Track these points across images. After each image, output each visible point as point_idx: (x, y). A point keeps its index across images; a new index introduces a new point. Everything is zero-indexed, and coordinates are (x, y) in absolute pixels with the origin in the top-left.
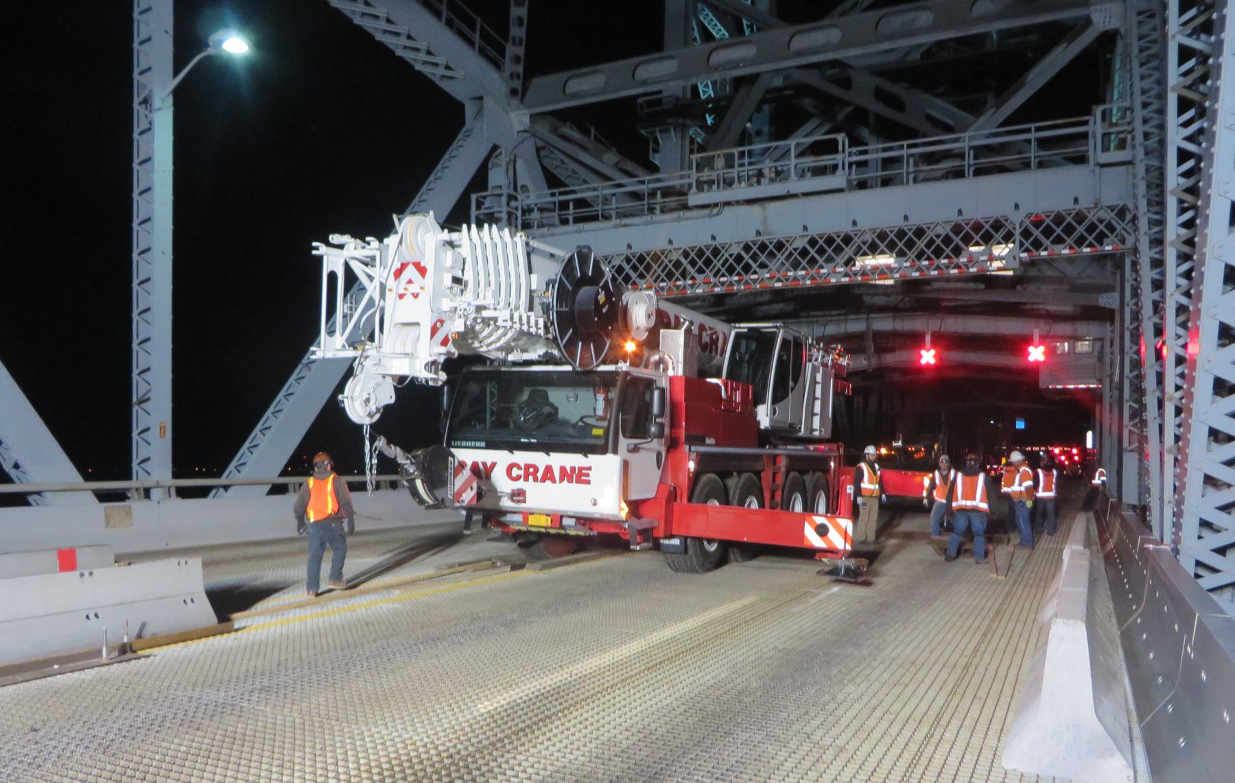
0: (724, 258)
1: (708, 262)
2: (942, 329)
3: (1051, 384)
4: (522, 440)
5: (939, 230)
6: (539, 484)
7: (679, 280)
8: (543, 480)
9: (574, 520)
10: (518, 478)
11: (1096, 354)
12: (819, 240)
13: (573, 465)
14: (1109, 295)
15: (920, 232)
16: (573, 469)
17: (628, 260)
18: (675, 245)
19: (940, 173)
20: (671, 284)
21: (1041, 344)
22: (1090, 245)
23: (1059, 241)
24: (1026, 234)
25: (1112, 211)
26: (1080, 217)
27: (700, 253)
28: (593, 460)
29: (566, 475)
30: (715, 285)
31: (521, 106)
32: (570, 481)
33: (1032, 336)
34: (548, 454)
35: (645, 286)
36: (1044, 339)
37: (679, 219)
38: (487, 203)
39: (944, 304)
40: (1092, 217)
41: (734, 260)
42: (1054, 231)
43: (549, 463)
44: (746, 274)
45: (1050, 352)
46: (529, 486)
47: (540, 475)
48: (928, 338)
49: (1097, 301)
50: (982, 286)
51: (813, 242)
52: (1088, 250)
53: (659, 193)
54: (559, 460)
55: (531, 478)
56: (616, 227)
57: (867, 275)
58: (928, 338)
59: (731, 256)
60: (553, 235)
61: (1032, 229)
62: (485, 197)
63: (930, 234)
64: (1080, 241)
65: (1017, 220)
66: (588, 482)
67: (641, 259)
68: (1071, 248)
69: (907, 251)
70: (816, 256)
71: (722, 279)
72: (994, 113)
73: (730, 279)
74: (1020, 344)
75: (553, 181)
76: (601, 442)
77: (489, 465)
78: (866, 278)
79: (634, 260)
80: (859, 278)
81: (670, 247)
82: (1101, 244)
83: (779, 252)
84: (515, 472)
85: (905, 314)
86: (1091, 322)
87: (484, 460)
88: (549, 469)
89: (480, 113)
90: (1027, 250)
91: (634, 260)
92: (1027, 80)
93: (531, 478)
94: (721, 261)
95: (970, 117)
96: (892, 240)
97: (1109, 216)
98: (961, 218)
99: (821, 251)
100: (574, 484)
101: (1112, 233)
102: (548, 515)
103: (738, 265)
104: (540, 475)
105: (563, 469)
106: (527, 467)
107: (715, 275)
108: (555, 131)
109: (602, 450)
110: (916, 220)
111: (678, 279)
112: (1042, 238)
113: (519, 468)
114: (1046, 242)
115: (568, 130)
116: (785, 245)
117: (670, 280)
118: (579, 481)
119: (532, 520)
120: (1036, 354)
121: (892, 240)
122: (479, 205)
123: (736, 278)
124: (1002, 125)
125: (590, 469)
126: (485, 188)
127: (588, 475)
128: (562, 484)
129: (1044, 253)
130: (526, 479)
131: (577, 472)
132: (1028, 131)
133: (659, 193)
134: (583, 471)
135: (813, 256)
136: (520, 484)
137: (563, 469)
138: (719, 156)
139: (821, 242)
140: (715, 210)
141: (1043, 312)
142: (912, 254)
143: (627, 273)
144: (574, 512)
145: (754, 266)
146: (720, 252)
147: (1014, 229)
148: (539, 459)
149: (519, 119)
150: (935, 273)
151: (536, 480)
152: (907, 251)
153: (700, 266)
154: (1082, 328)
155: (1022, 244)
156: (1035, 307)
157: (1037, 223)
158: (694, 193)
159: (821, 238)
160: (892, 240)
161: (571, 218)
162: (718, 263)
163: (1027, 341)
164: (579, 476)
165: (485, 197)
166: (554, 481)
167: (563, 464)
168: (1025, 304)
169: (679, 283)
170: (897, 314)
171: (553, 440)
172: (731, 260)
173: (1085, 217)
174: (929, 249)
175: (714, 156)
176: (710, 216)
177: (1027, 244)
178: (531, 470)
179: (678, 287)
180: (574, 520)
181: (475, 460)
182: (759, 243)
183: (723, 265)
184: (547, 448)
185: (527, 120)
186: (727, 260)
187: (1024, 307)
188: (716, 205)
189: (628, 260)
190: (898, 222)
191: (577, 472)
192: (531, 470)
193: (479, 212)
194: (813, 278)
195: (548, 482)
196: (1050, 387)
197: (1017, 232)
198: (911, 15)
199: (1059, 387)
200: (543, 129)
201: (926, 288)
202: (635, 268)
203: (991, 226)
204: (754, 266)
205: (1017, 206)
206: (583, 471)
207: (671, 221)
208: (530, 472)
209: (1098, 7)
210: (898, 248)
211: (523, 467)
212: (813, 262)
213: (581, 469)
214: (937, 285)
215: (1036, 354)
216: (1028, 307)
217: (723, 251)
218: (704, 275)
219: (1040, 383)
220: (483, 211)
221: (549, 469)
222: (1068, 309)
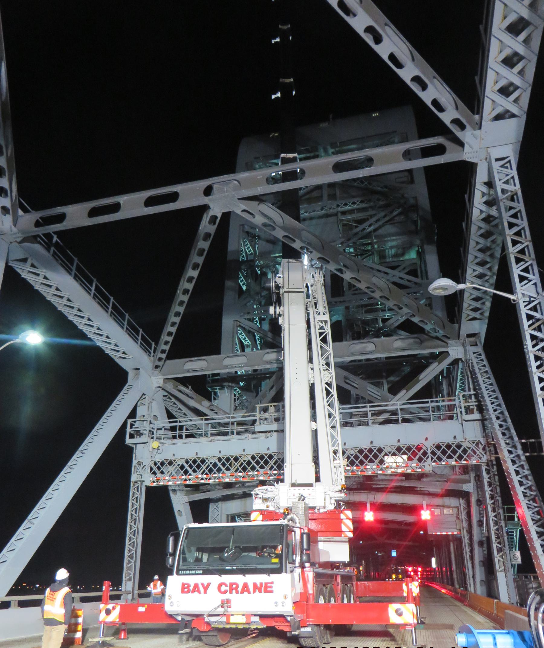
0: (241, 463)
1: (199, 467)
2: (375, 501)
3: (434, 532)
4: (227, 568)
5: (352, 452)
6: (240, 595)
7: (183, 475)
8: (242, 592)
9: (259, 617)
10: (225, 592)
11: (455, 515)
12: (265, 456)
13: (261, 581)
14: (468, 484)
15: (203, 461)
16: (261, 584)
17: (187, 462)
18: (247, 452)
19: (381, 420)
20: (245, 474)
21: (427, 509)
22: (465, 460)
23: (450, 457)
24: (433, 453)
25: (474, 443)
26: (459, 446)
27: (262, 457)
28: (274, 577)
29: (257, 588)
30: (271, 475)
31: (159, 374)
32: (260, 591)
33: (423, 505)
34: (220, 576)
35: (230, 475)
36: (429, 506)
37: (249, 438)
38: (136, 425)
39: (374, 486)
40: (465, 445)
41: (246, 464)
42: (363, 457)
43: (245, 581)
44: (210, 474)
45: (432, 514)
46: (233, 597)
47: (240, 589)
48: (368, 505)
49: (462, 487)
50: (404, 478)
51: (253, 458)
52: (465, 462)
53: (235, 423)
54: (251, 579)
55: (234, 591)
56: (212, 441)
57: (354, 472)
58: (368, 505)
59: (211, 463)
60: (174, 444)
61: (422, 451)
62: (135, 422)
63: (241, 460)
64: (460, 457)
65: (429, 446)
66: (272, 592)
67: (228, 459)
68: (456, 461)
69: (453, 456)
70: (458, 454)
71: (215, 475)
72: (406, 393)
73: (279, 472)
74: (414, 509)
75: (170, 415)
76: (278, 566)
77: (206, 585)
78: (354, 473)
79: (191, 462)
80: (350, 474)
81: (244, 453)
82: (470, 459)
83: (203, 464)
84: (223, 588)
85: (355, 492)
86: (451, 498)
87: (202, 582)
88: (245, 585)
89: (137, 376)
90: (435, 461)
91: (191, 462)
92: (420, 378)
93: (234, 591)
94: (239, 464)
95: (392, 396)
96: (366, 454)
97: (473, 446)
98: (372, 445)
99: (366, 457)
100: (263, 594)
101: (475, 455)
102: (243, 615)
103: (213, 468)
104: (240, 589)
105: (255, 585)
106: (231, 584)
107: (202, 474)
108: (175, 387)
109: (278, 571)
110: (202, 455)
111: (249, 471)
112: (442, 456)
113: (226, 585)
114: (444, 458)
115: (182, 388)
116: (239, 459)
117: (186, 475)
118: (266, 591)
119: (233, 620)
120: (425, 515)
121: (366, 454)
122: (132, 425)
123: (256, 473)
124: (410, 399)
125: (272, 583)
126: (135, 417)
127: (271, 587)
128: (255, 594)
129: (444, 463)
130: (231, 592)
131: (264, 586)
132: (427, 402)
133: (235, 423)
134: (268, 585)
135: (253, 465)
136: (227, 596)
137: (255, 585)
138: (271, 406)
139: (258, 458)
140: (269, 434)
141: (426, 492)
142: (267, 468)
143: (186, 469)
144: (247, 612)
145: (258, 467)
146: (239, 459)
147: (427, 450)
148: (239, 579)
149: (157, 380)
150: (380, 472)
151: (237, 592)
152: (453, 456)
153: (262, 464)
154: (448, 501)
155: (432, 459)
156: (422, 489)
157: (438, 447)
158: (258, 425)
159: (266, 455)
160: (366, 454)
161: (184, 435)
162: (204, 467)
163: (421, 507)
164: (266, 588)
165: (135, 422)
166: (249, 592)
167: (254, 582)
168: (417, 487)
169: (249, 473)
170: (351, 492)
171: (248, 567)
172: (211, 466)
173: (461, 446)
174: (275, 465)
175: (268, 406)
176: (266, 437)
177: (435, 458)
178: (234, 586)
179: (249, 476)
180: (259, 617)
181: (196, 582)
182: (268, 454)
183: (207, 468)
184: (244, 572)
185: (161, 381)
186: (209, 466)
187: (416, 489)
188: (270, 432)
189: (220, 460)
190: (368, 446)
191: (264, 586)
192: (234, 586)
193: (131, 430)
194: (362, 471)
195: (246, 593)
196: (434, 533)
197: (429, 452)
198: (364, 345)
199: (439, 533)
200: (170, 387)
201: (376, 478)
202: (191, 467)
203: (416, 448)
204: (258, 467)
205: (427, 439)
206: (268, 585)
207: (263, 437)
208: (233, 587)
209: (452, 348)
210: (448, 454)
211: (228, 584)
212: (362, 463)
213: (266, 584)
214: (380, 477)
215: (425, 515)
216: (418, 489)
217: (207, 461)
218: (264, 469)
219: (429, 532)
220: (133, 429)
221: (245, 585)
222: (438, 490)
